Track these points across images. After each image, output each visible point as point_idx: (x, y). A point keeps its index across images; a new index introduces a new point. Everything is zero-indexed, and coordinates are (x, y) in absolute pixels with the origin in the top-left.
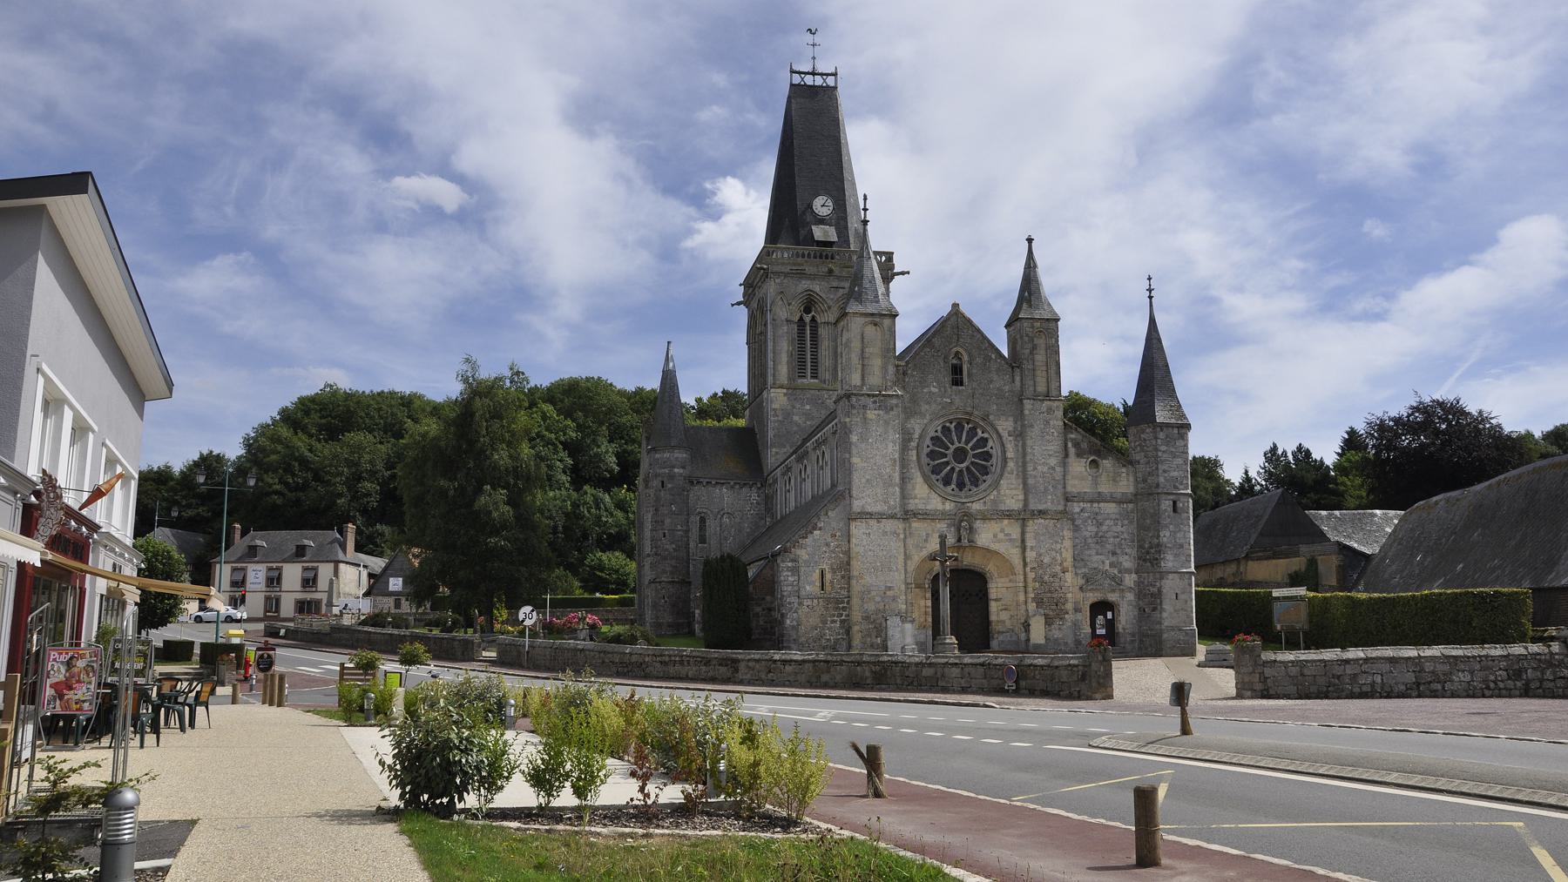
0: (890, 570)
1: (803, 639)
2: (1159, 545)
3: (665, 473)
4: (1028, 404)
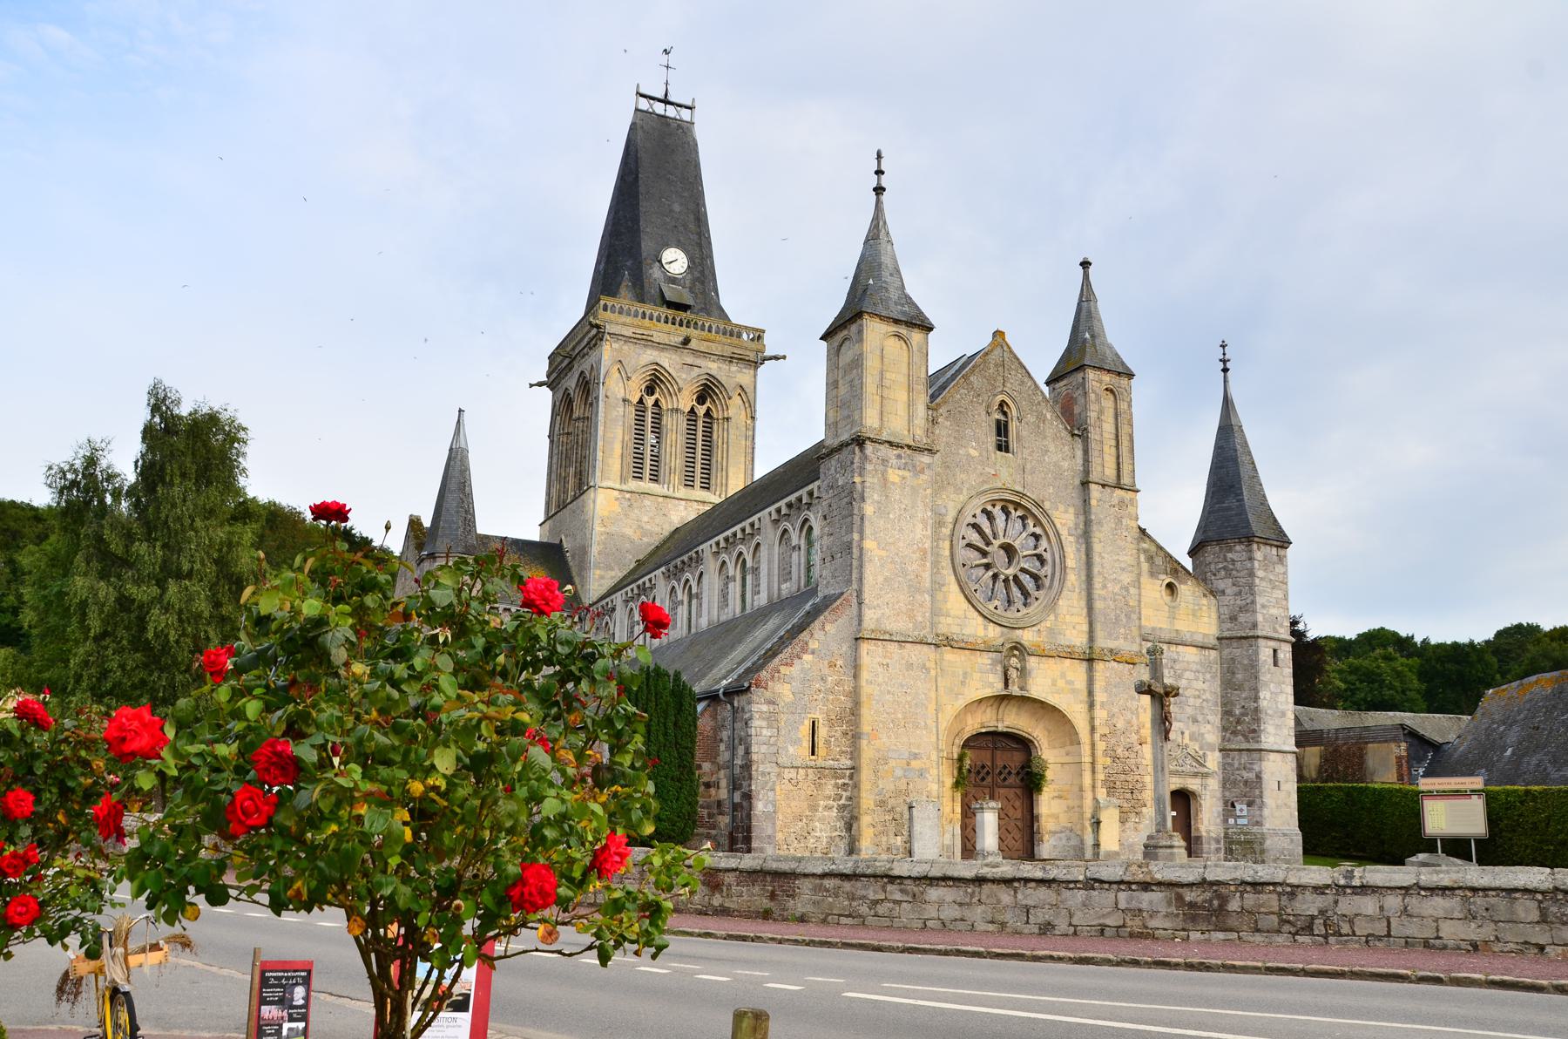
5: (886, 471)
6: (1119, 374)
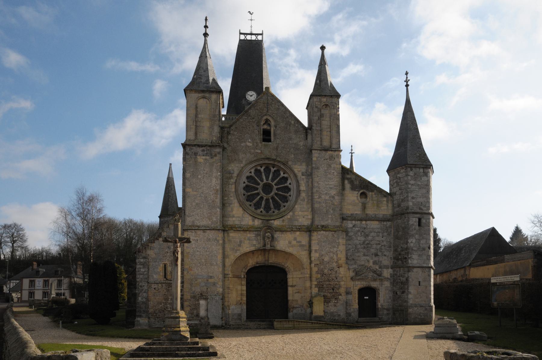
0: (212, 265)
1: (151, 310)
2: (407, 249)
4: (315, 154)
6: (331, 96)
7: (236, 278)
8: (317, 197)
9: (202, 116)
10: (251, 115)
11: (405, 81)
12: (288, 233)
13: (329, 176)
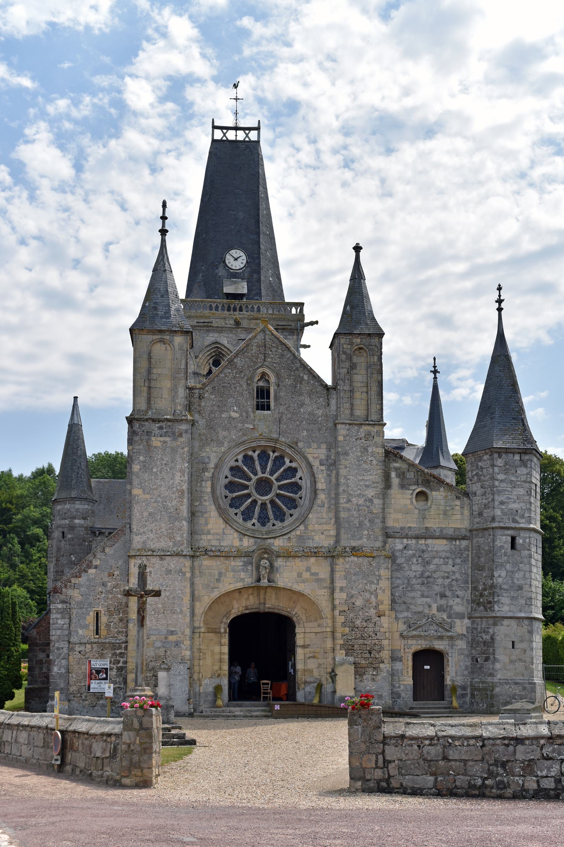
2: (492, 586)
3: (66, 524)
4: (342, 430)
5: (150, 439)
7: (212, 632)
8: (345, 500)
9: (159, 371)
10: (238, 367)
11: (496, 302)
12: (297, 560)
13: (365, 466)
